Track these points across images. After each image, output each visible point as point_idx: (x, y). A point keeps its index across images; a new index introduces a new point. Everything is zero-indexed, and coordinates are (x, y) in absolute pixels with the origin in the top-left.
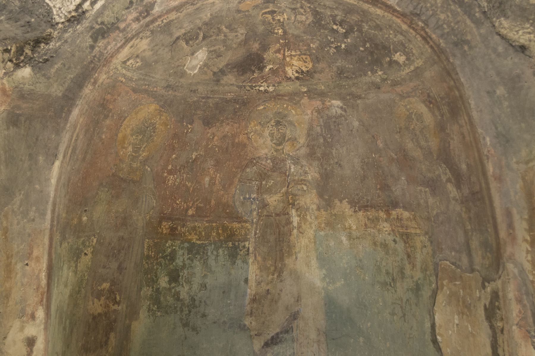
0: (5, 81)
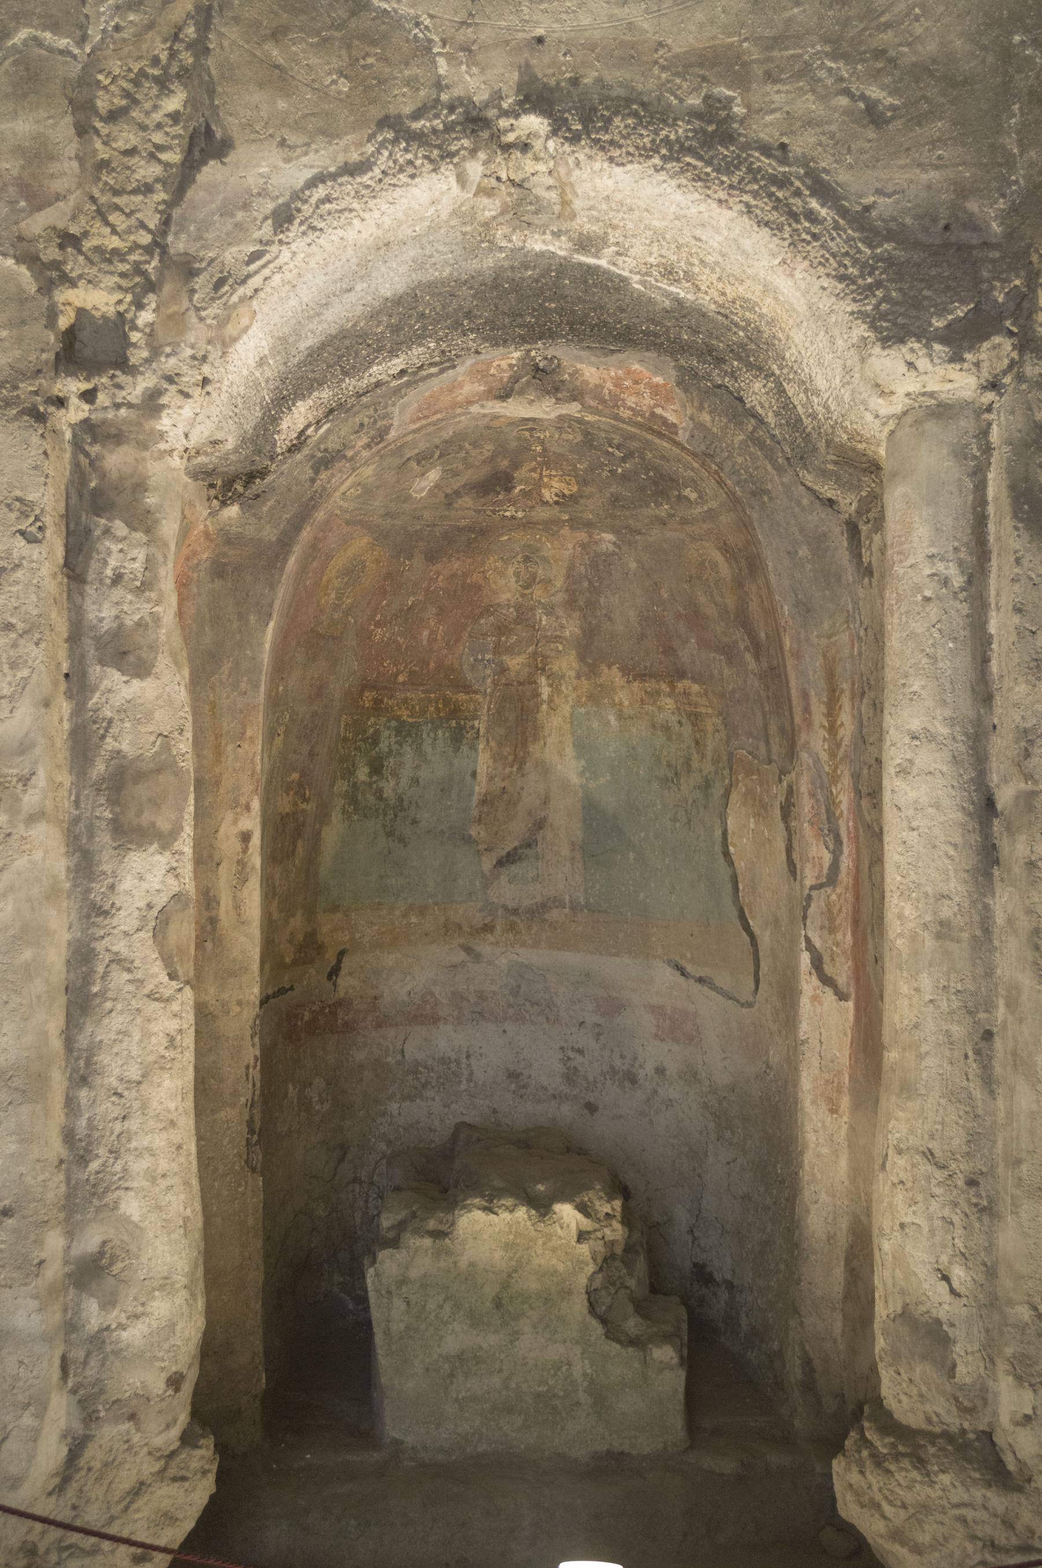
0: (208, 523)
